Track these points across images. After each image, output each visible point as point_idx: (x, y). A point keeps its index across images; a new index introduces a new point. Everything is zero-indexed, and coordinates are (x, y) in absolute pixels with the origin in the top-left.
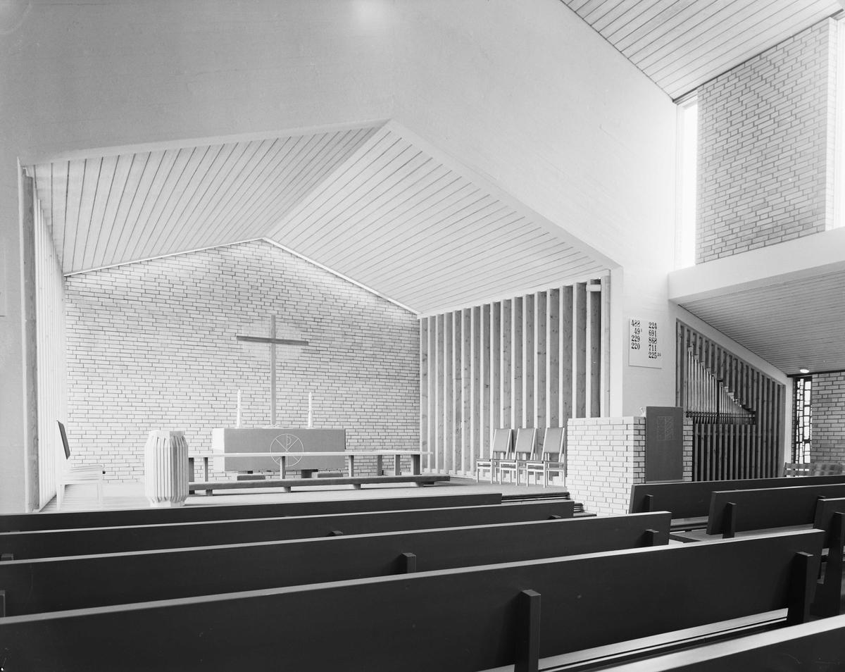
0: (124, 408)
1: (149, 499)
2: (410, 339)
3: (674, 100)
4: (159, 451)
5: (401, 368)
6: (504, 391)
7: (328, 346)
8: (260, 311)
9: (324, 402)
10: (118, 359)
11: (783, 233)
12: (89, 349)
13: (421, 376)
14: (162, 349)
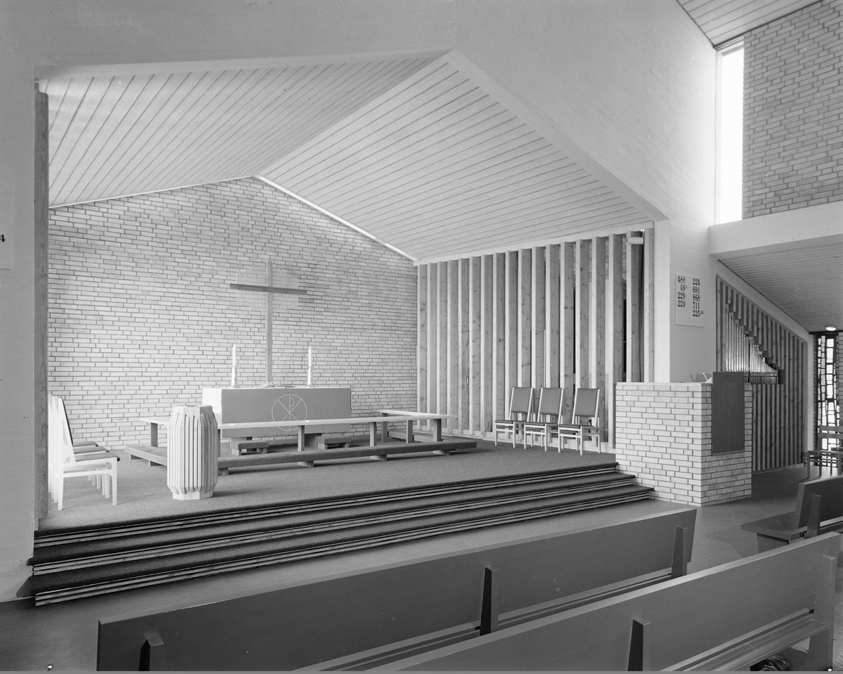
0: (97, 364)
1: (172, 490)
2: (406, 287)
3: (715, 46)
4: (187, 429)
5: (397, 318)
6: (523, 347)
7: (322, 294)
8: (250, 255)
10: (92, 308)
13: (419, 327)
14: (143, 297)
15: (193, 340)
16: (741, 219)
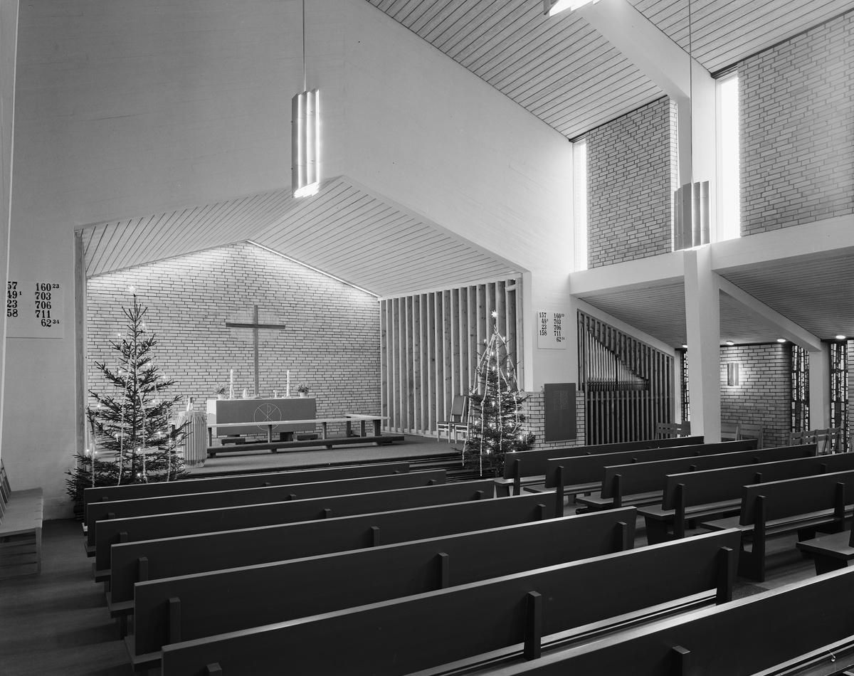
7: (302, 326)
8: (245, 300)
9: (299, 373)
11: (645, 251)
12: (105, 337)
14: (164, 335)
15: (201, 364)
16: (739, 237)
